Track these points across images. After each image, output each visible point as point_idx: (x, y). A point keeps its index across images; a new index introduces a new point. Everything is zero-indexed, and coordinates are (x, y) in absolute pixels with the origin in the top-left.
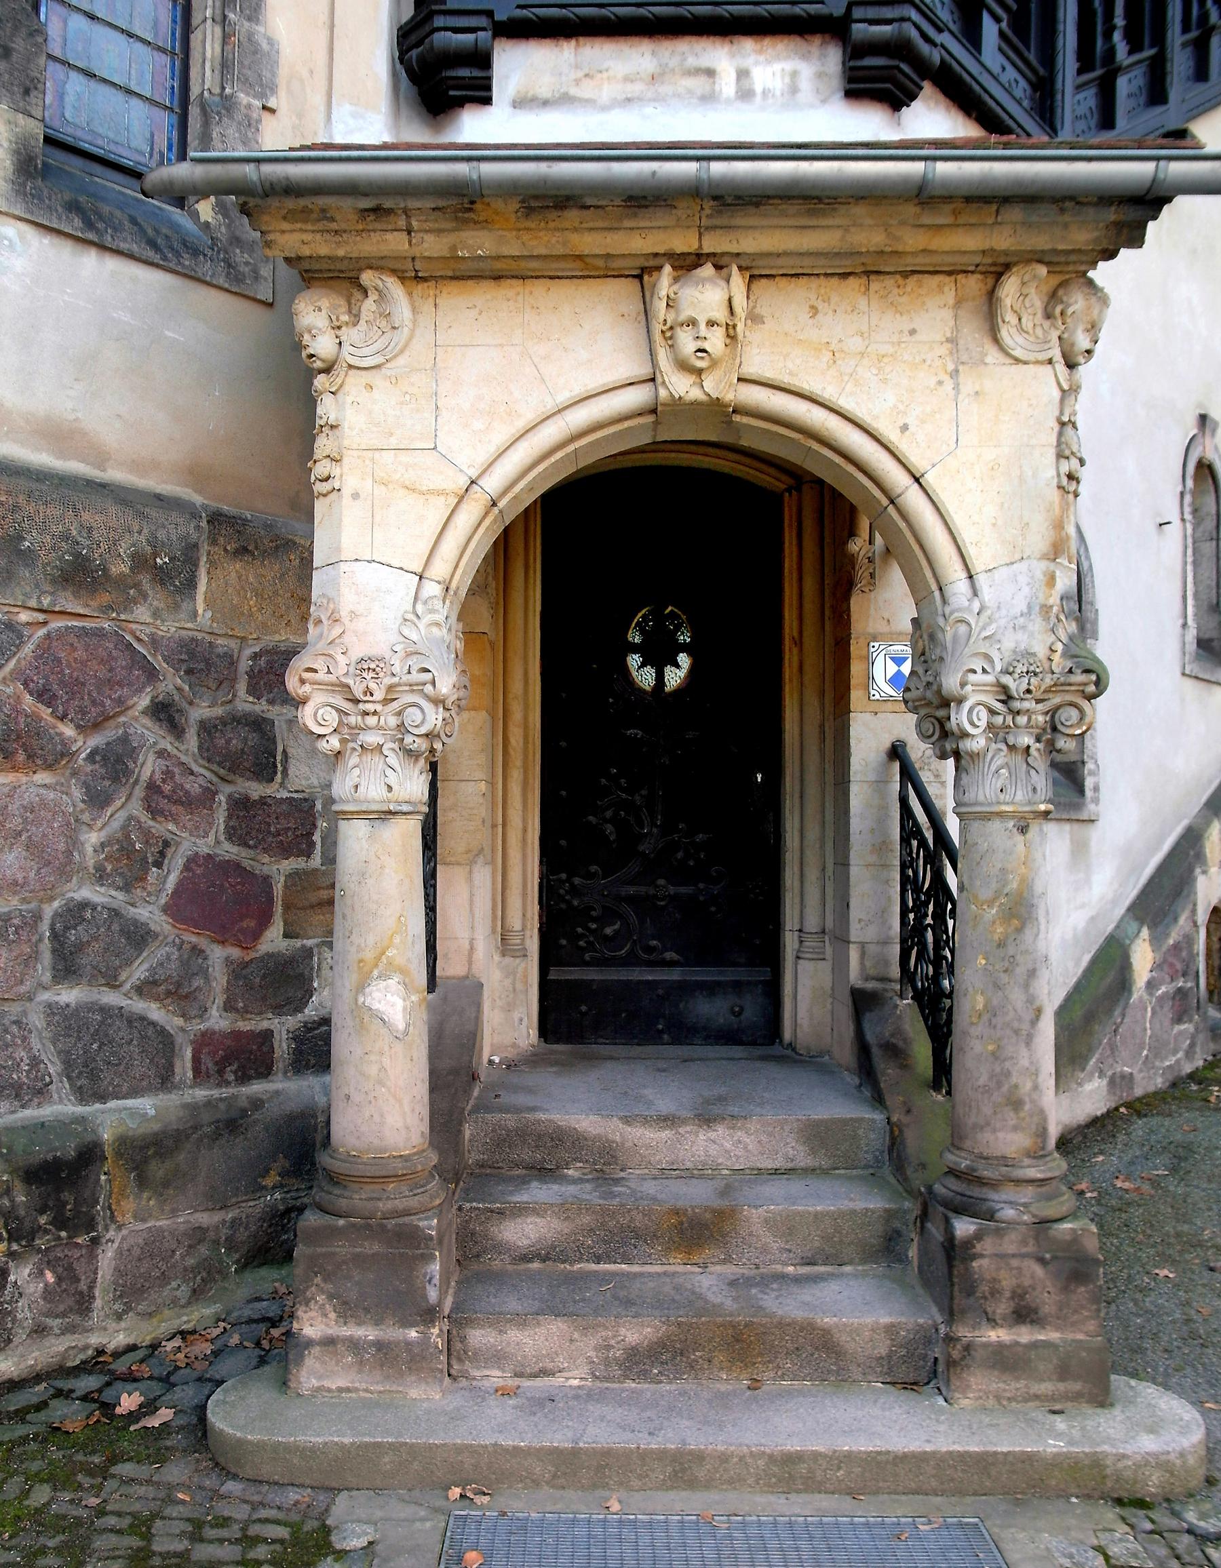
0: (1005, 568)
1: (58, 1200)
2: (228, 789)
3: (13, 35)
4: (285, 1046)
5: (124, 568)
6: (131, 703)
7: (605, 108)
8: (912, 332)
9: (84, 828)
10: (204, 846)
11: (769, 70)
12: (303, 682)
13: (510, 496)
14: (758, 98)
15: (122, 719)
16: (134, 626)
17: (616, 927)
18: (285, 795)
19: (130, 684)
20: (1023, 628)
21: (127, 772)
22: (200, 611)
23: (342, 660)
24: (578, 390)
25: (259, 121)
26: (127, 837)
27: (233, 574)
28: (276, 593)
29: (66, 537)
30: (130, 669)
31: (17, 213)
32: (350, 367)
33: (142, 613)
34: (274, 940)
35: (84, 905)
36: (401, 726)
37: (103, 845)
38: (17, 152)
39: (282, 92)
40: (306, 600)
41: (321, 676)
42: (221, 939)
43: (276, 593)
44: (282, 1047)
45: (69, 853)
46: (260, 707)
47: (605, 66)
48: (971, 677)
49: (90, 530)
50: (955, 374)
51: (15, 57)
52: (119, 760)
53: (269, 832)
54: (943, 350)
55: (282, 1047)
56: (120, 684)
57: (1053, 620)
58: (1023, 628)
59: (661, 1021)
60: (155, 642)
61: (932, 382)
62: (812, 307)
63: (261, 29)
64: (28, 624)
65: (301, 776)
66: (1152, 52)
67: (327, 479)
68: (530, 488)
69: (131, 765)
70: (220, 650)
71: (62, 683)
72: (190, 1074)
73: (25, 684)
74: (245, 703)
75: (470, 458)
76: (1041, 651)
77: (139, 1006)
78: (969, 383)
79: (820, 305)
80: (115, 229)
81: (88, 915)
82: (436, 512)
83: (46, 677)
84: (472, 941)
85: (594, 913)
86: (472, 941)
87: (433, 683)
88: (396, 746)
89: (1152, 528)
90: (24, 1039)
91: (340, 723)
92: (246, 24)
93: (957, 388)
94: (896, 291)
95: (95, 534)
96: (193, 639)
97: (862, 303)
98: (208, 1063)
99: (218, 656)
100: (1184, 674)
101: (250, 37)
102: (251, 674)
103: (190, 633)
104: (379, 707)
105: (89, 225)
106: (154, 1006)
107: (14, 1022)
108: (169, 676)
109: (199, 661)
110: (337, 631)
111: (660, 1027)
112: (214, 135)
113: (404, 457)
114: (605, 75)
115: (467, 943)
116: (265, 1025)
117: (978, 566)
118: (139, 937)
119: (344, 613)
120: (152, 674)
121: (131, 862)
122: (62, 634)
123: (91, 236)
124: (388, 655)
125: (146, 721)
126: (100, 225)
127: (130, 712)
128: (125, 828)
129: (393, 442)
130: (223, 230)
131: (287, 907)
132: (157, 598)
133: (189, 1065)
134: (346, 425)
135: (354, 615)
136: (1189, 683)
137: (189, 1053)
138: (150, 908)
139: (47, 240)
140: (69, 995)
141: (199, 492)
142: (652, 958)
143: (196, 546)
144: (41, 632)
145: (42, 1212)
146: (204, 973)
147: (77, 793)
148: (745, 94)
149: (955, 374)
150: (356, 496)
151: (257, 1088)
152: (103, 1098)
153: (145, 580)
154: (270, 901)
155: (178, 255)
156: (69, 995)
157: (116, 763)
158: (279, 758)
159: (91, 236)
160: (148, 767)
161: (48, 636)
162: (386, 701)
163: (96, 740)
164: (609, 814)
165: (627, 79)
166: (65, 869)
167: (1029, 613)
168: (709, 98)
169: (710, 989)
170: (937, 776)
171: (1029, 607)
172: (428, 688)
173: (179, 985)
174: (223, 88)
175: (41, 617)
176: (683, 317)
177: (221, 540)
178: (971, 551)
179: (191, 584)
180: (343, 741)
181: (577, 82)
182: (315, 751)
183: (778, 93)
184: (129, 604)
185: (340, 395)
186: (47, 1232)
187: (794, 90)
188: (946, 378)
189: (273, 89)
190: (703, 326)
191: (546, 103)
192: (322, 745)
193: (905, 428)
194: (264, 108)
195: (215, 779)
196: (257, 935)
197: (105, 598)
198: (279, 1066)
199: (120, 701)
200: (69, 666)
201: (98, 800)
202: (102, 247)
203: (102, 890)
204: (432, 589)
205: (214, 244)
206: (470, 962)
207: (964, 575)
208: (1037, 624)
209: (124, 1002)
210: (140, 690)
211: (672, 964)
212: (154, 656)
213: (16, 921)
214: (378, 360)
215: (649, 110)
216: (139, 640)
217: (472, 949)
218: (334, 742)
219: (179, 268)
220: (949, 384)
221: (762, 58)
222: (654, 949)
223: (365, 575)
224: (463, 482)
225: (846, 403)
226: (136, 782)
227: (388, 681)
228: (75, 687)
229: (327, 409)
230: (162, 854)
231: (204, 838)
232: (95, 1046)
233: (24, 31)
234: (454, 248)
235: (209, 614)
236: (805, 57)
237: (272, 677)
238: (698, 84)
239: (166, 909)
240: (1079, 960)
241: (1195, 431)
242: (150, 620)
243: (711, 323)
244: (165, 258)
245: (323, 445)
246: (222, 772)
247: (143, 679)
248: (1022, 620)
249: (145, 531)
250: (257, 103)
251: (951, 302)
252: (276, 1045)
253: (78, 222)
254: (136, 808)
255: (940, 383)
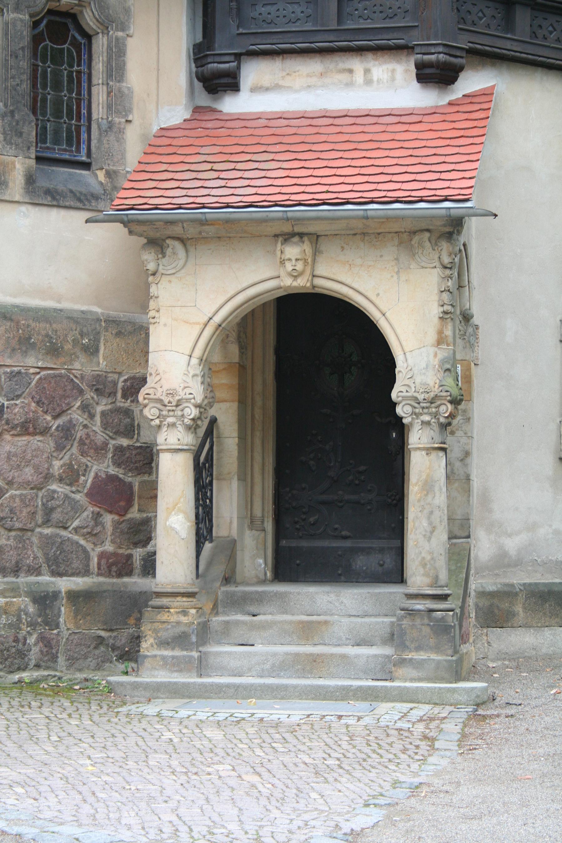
0: (417, 351)
1: (45, 613)
2: (113, 442)
3: (23, 126)
4: (138, 562)
5: (70, 347)
6: (72, 404)
7: (296, 91)
8: (381, 256)
9: (54, 459)
10: (103, 467)
11: (381, 69)
12: (145, 399)
13: (226, 322)
14: (375, 83)
15: (69, 412)
16: (74, 371)
17: (316, 517)
18: (138, 444)
19: (72, 396)
20: (424, 374)
21: (72, 436)
22: (101, 362)
23: (160, 390)
24: (251, 282)
25: (124, 129)
26: (71, 462)
27: (115, 344)
28: (134, 350)
29: (47, 335)
30: (72, 390)
31: (26, 201)
32: (162, 274)
34: (134, 514)
35: (54, 491)
36: (183, 416)
37: (62, 466)
38: (26, 175)
39: (135, 111)
40: (147, 361)
42: (110, 509)
43: (134, 350)
44: (137, 562)
45: (48, 469)
46: (128, 404)
47: (297, 69)
48: (400, 394)
49: (56, 331)
50: (398, 273)
51: (24, 135)
52: (68, 430)
53: (132, 462)
54: (393, 263)
55: (137, 562)
56: (68, 397)
57: (436, 371)
58: (424, 374)
59: (340, 569)
60: (82, 378)
62: (342, 247)
64: (33, 373)
65: (145, 437)
67: (154, 318)
68: (236, 317)
69: (73, 432)
70: (109, 379)
71: (46, 398)
72: (96, 569)
73: (32, 398)
74: (121, 403)
76: (432, 384)
77: (76, 538)
79: (345, 246)
80: (64, 197)
81: (56, 496)
82: (196, 330)
83: (40, 396)
84: (231, 518)
85: (304, 510)
86: (231, 518)
87: (194, 398)
88: (181, 423)
90: (31, 547)
91: (160, 414)
92: (118, 84)
94: (375, 240)
95: (58, 333)
96: (98, 375)
97: (362, 244)
99: (109, 382)
101: (120, 90)
102: (123, 389)
103: (97, 373)
104: (174, 408)
105: (54, 198)
106: (81, 538)
107: (28, 539)
108: (88, 392)
109: (102, 386)
110: (158, 378)
111: (340, 572)
112: (104, 142)
114: (297, 74)
115: (228, 519)
116: (129, 551)
117: (407, 349)
118: (76, 508)
119: (161, 371)
120: (81, 392)
122: (45, 378)
123: (55, 203)
124: (178, 388)
125: (79, 412)
126: (58, 197)
127: (72, 409)
128: (71, 459)
130: (109, 185)
131: (140, 497)
132: (83, 358)
133: (96, 566)
134: (161, 297)
135: (165, 372)
137: (96, 560)
138: (81, 494)
139: (37, 209)
140: (47, 531)
142: (335, 534)
143: (99, 333)
144: (38, 377)
145: (39, 617)
146: (103, 525)
147: (52, 444)
148: (368, 82)
149: (398, 273)
150: (165, 325)
151: (126, 580)
152: (61, 575)
153: (77, 350)
154: (132, 494)
155: (89, 201)
156: (47, 531)
157: (67, 431)
158: (136, 428)
159: (55, 203)
160: (80, 433)
161: (40, 378)
162: (177, 406)
163: (60, 421)
164: (312, 456)
165: (308, 76)
167: (427, 368)
168: (350, 84)
169: (367, 551)
170: (465, 433)
171: (427, 366)
172: (193, 401)
174: (108, 118)
175: (38, 370)
176: (286, 258)
177: (110, 330)
178: (404, 344)
180: (161, 422)
181: (283, 78)
183: (385, 81)
184: (71, 362)
185: (159, 285)
186: (41, 625)
187: (393, 79)
188: (395, 275)
189: (130, 111)
190: (294, 261)
191: (267, 89)
192: (153, 423)
193: (378, 295)
194: (127, 121)
195: (108, 438)
196: (126, 510)
197: (63, 359)
198: (137, 571)
199: (68, 404)
200: (49, 390)
201: (60, 448)
202: (58, 206)
203: (61, 485)
204: (195, 361)
205: (105, 192)
206: (230, 530)
207: (402, 353)
208: (431, 373)
209: (70, 535)
210: (76, 399)
211: (345, 538)
212: (82, 383)
213: (29, 497)
214: (173, 271)
215: (319, 92)
216: (76, 377)
217: (231, 523)
218: (157, 422)
219: (90, 208)
220: (395, 277)
221: (377, 63)
222: (336, 529)
224: (206, 319)
226: (75, 439)
228: (52, 399)
229: (153, 290)
230: (85, 470)
232: (58, 552)
233: (27, 123)
234: (200, 233)
235: (105, 363)
237: (133, 390)
238: (344, 77)
239: (87, 495)
243: (297, 260)
244: (84, 205)
245: (152, 304)
246: (111, 434)
247: (77, 394)
248: (424, 371)
249: (78, 329)
250: (124, 120)
251: (396, 243)
252: (134, 561)
253: (49, 198)
255: (392, 276)
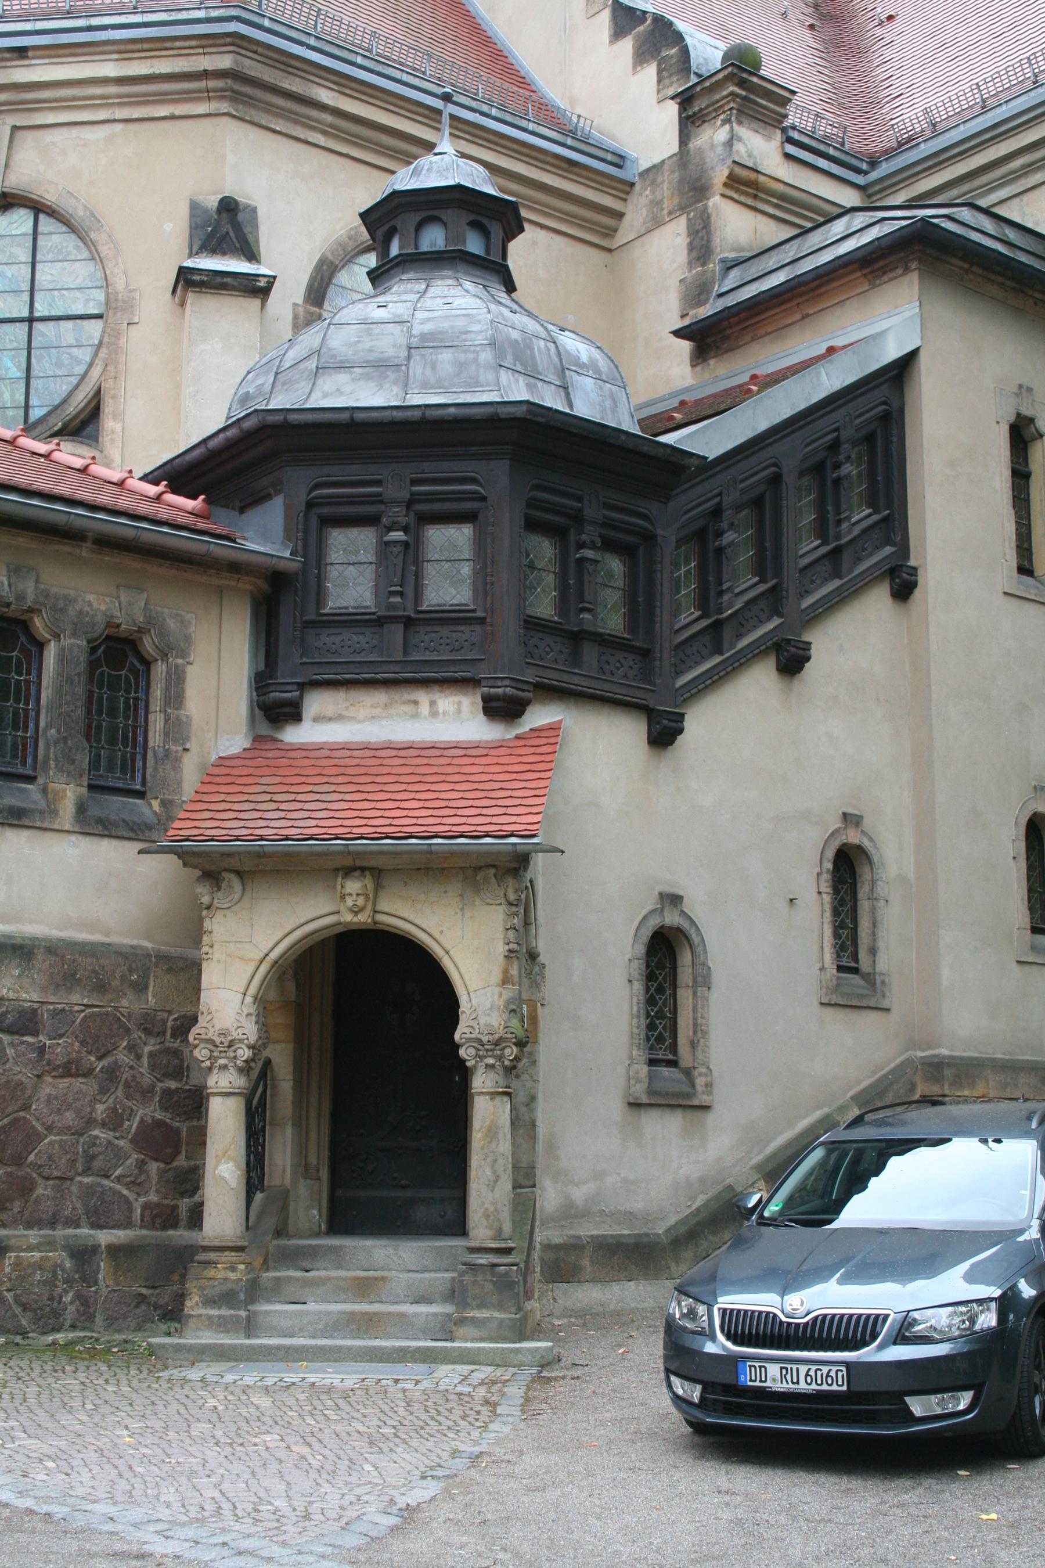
2: (161, 1085)
7: (360, 722)
18: (188, 1087)
23: (212, 1030)
24: (310, 917)
26: (115, 1106)
29: (94, 971)
33: (124, 1003)
34: (181, 1162)
39: (193, 739)
41: (203, 1037)
45: (91, 1113)
52: (114, 1071)
61: (453, 913)
63: (183, 712)
65: (195, 1079)
66: (775, 581)
74: (171, 1044)
75: (265, 947)
78: (468, 914)
84: (284, 1166)
89: (784, 905)
93: (463, 915)
98: (147, 1219)
100: (822, 1004)
101: (178, 718)
102: (173, 1028)
105: (105, 828)
113: (239, 945)
117: (471, 989)
119: (213, 1010)
120: (128, 1031)
121: (115, 1121)
122: (92, 1016)
129: (234, 939)
131: (187, 1144)
132: (131, 995)
136: (829, 1012)
137: (139, 1210)
141: (150, 941)
144: (83, 1014)
148: (434, 714)
149: (462, 909)
159: (106, 833)
160: (126, 1075)
161: (85, 1016)
162: (229, 1047)
166: (91, 1122)
168: (415, 716)
172: (246, 1041)
173: (136, 1178)
175: (83, 1008)
179: (146, 987)
181: (347, 708)
182: (201, 1068)
187: (459, 711)
191: (330, 719)
192: (203, 1065)
193: (442, 932)
198: (183, 1223)
199: (114, 1044)
201: (103, 1090)
210: (122, 1039)
211: (404, 1187)
215: (384, 723)
216: (123, 1015)
218: (208, 1063)
223: (221, 993)
224: (262, 955)
225: (418, 922)
227: (230, 1038)
229: (207, 924)
230: (130, 1115)
231: (150, 1111)
236: (465, 694)
238: (409, 709)
239: (131, 1141)
240: (693, 1198)
241: (838, 825)
242: (128, 1003)
243: (358, 895)
245: (205, 939)
250: (181, 748)
253: (100, 828)
254: (120, 1093)
